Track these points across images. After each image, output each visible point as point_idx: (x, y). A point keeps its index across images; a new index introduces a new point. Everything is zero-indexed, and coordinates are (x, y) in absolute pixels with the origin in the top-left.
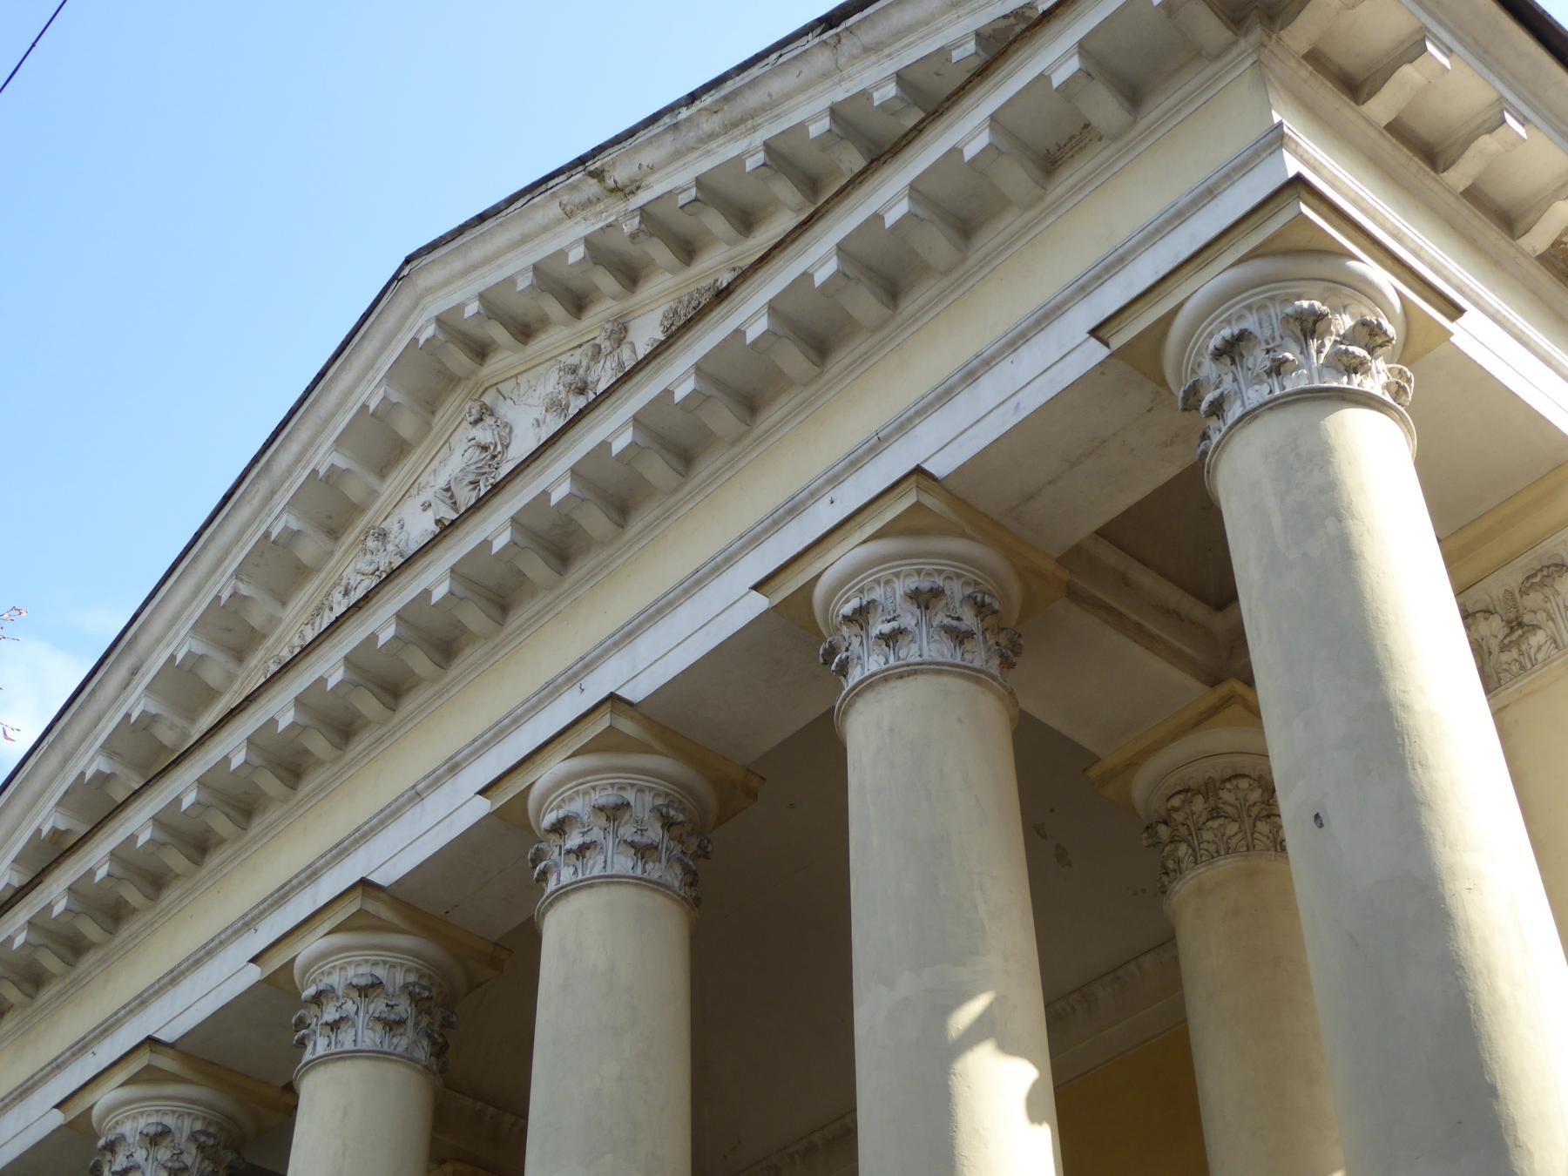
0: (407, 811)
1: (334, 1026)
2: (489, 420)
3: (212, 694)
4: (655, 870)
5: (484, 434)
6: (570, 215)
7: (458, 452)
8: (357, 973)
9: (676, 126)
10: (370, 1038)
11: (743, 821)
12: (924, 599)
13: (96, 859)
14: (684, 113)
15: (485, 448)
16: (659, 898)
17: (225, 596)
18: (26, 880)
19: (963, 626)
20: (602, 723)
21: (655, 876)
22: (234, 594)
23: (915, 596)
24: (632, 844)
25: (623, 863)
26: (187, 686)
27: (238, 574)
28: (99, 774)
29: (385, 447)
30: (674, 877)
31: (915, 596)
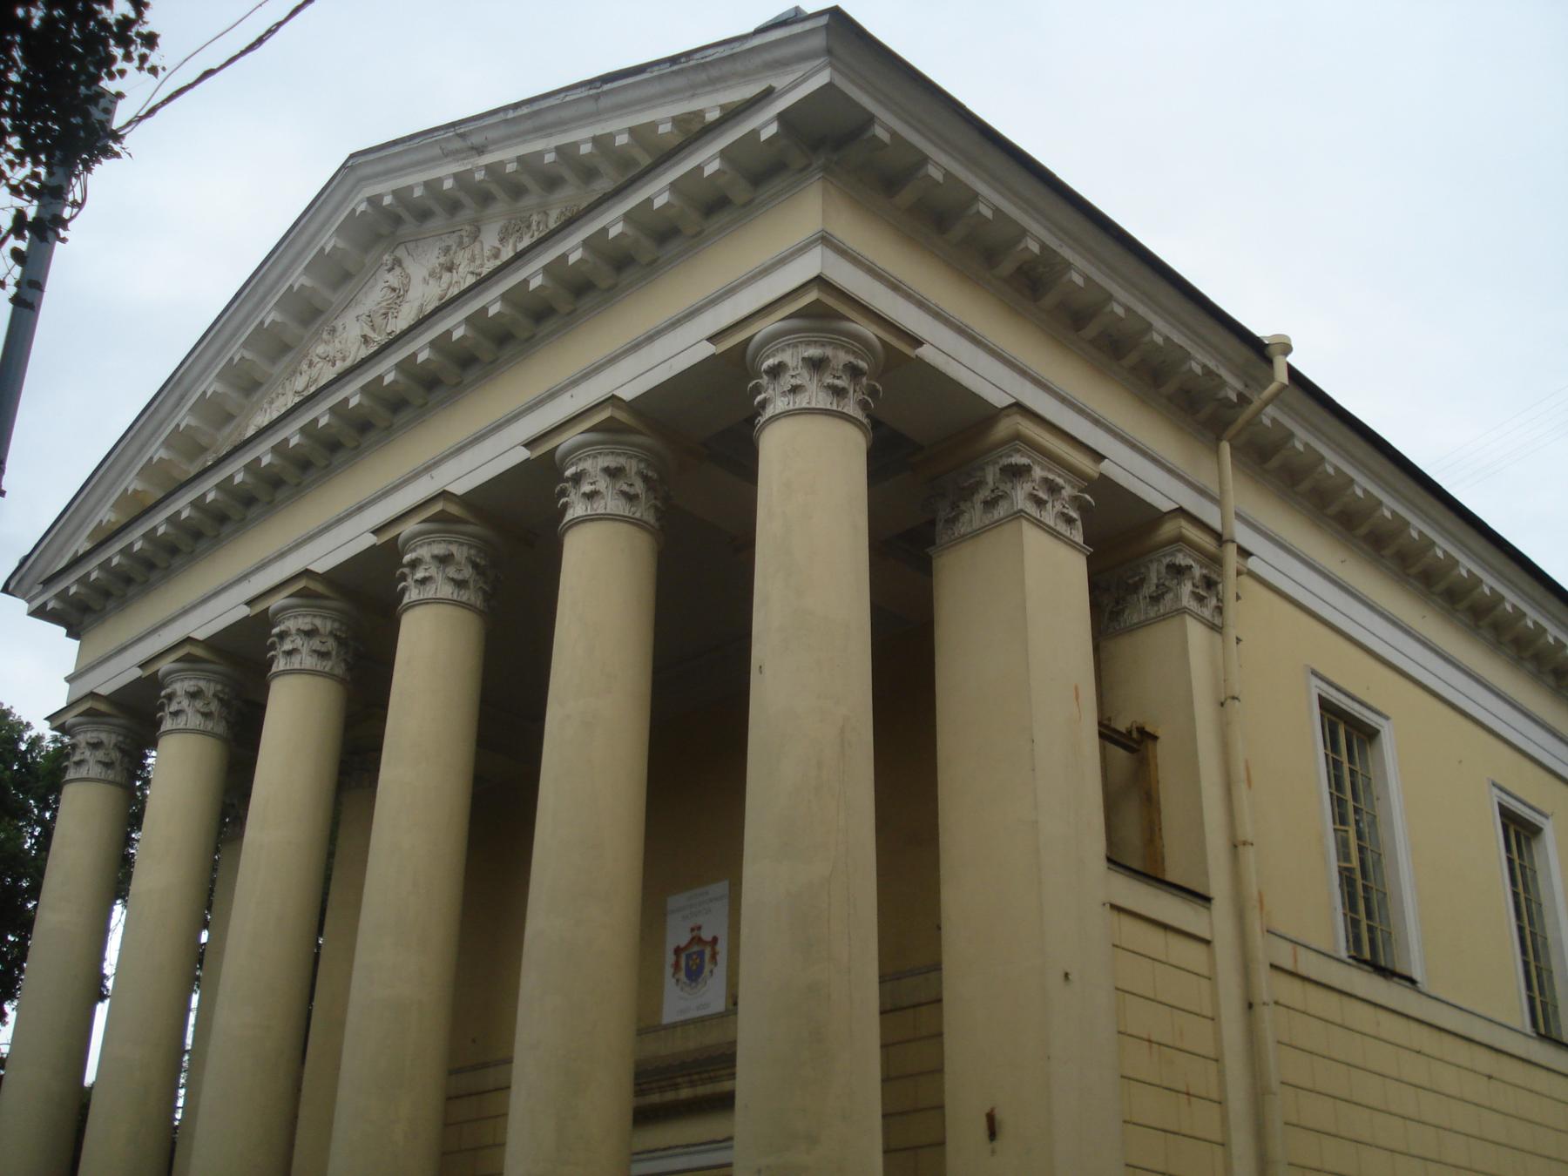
0: (329, 532)
1: (289, 653)
2: (398, 270)
3: (203, 450)
4: (465, 596)
5: (393, 279)
6: (446, 155)
7: (378, 288)
8: (304, 623)
9: (506, 121)
10: (309, 662)
11: (511, 539)
12: (613, 473)
13: (135, 539)
14: (511, 115)
15: (394, 290)
16: (465, 612)
17: (236, 359)
18: (124, 520)
19: (632, 491)
20: (437, 507)
21: (464, 599)
22: (242, 358)
23: (608, 471)
24: (452, 580)
25: (447, 591)
26: (187, 443)
27: (245, 345)
28: (135, 492)
29: (342, 275)
30: (477, 600)
31: (608, 471)
